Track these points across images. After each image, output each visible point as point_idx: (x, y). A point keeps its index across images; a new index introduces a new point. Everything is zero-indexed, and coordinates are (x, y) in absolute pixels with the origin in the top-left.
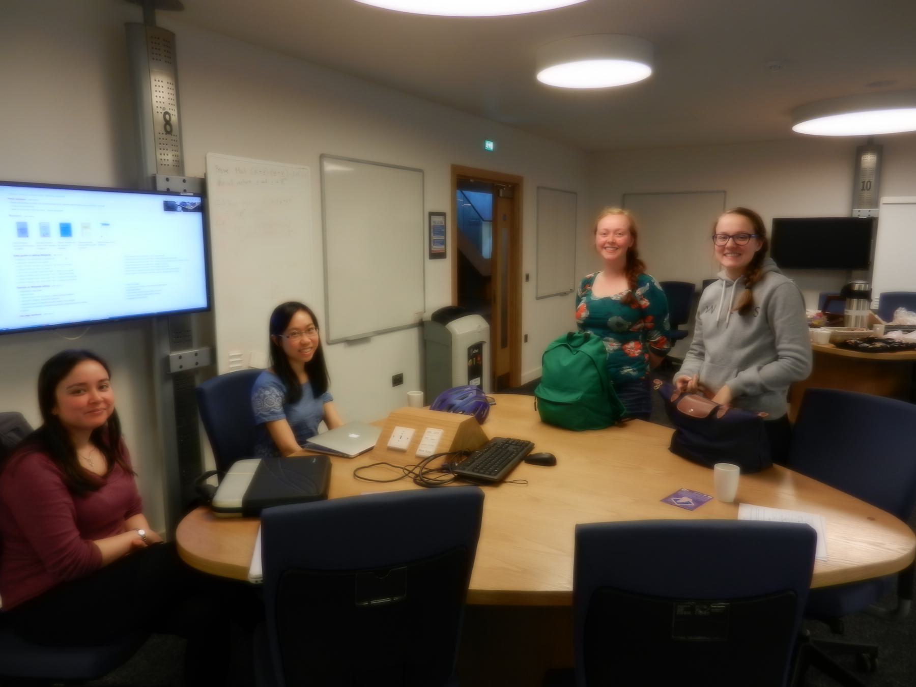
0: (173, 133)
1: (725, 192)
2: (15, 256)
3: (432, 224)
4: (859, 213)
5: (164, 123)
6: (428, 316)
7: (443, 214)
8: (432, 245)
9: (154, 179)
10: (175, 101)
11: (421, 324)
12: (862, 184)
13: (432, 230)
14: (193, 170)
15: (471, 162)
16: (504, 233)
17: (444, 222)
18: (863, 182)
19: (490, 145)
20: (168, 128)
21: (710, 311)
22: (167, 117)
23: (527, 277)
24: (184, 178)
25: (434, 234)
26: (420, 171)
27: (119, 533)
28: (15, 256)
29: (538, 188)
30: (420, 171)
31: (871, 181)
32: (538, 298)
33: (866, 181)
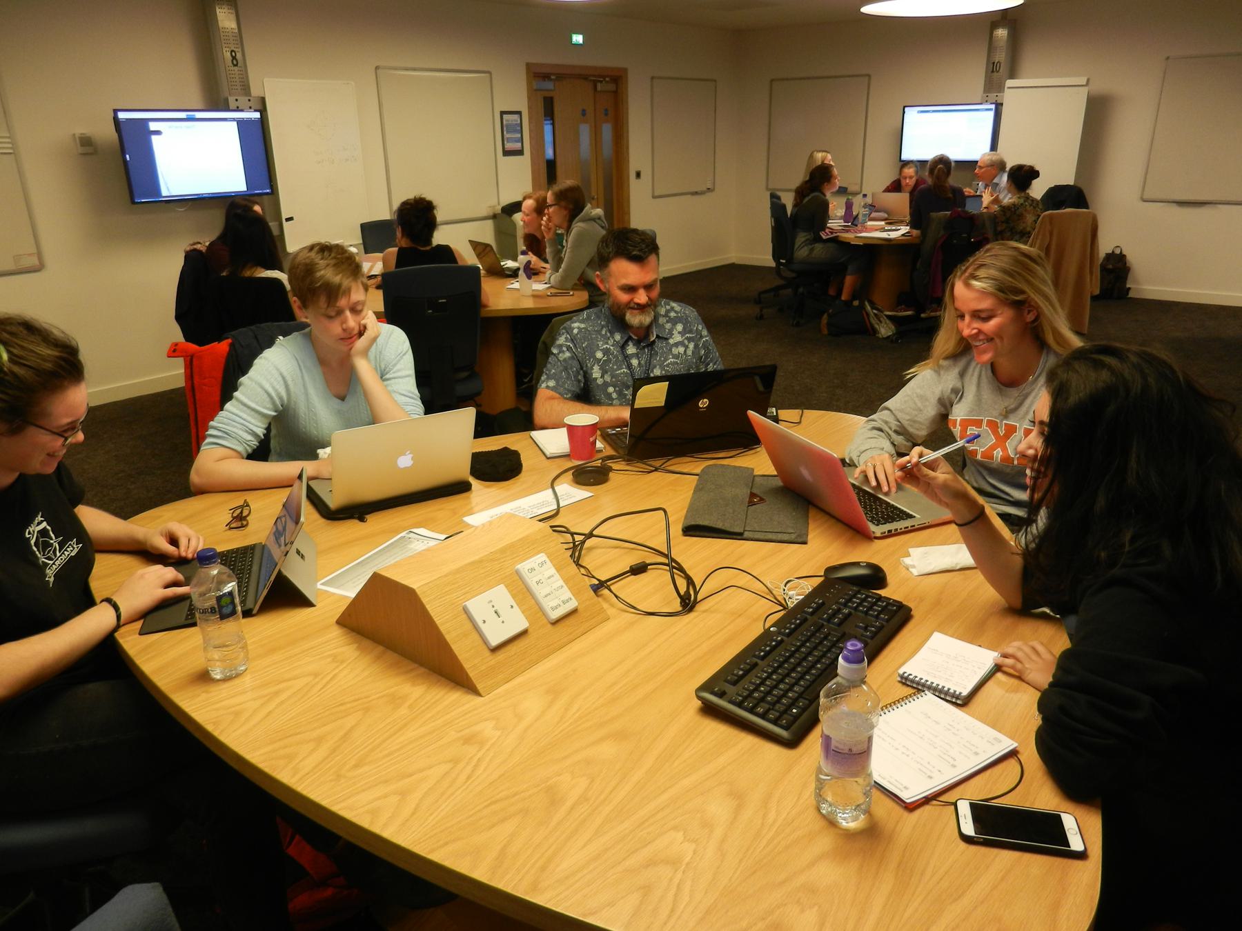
0: (239, 65)
1: (869, 76)
2: (303, 557)
3: (504, 122)
4: (997, 98)
5: (231, 58)
6: (498, 209)
7: (519, 113)
8: (505, 143)
9: (226, 100)
10: (238, 38)
11: (494, 217)
13: (505, 129)
14: (255, 92)
15: (549, 58)
16: (607, 130)
17: (519, 120)
18: (994, 63)
19: (578, 39)
20: (235, 62)
21: (77, 136)
22: (233, 54)
23: (638, 175)
24: (249, 98)
25: (507, 132)
26: (489, 72)
27: (342, 595)
28: (303, 557)
29: (653, 78)
30: (489, 72)
32: (654, 197)
33: (997, 61)
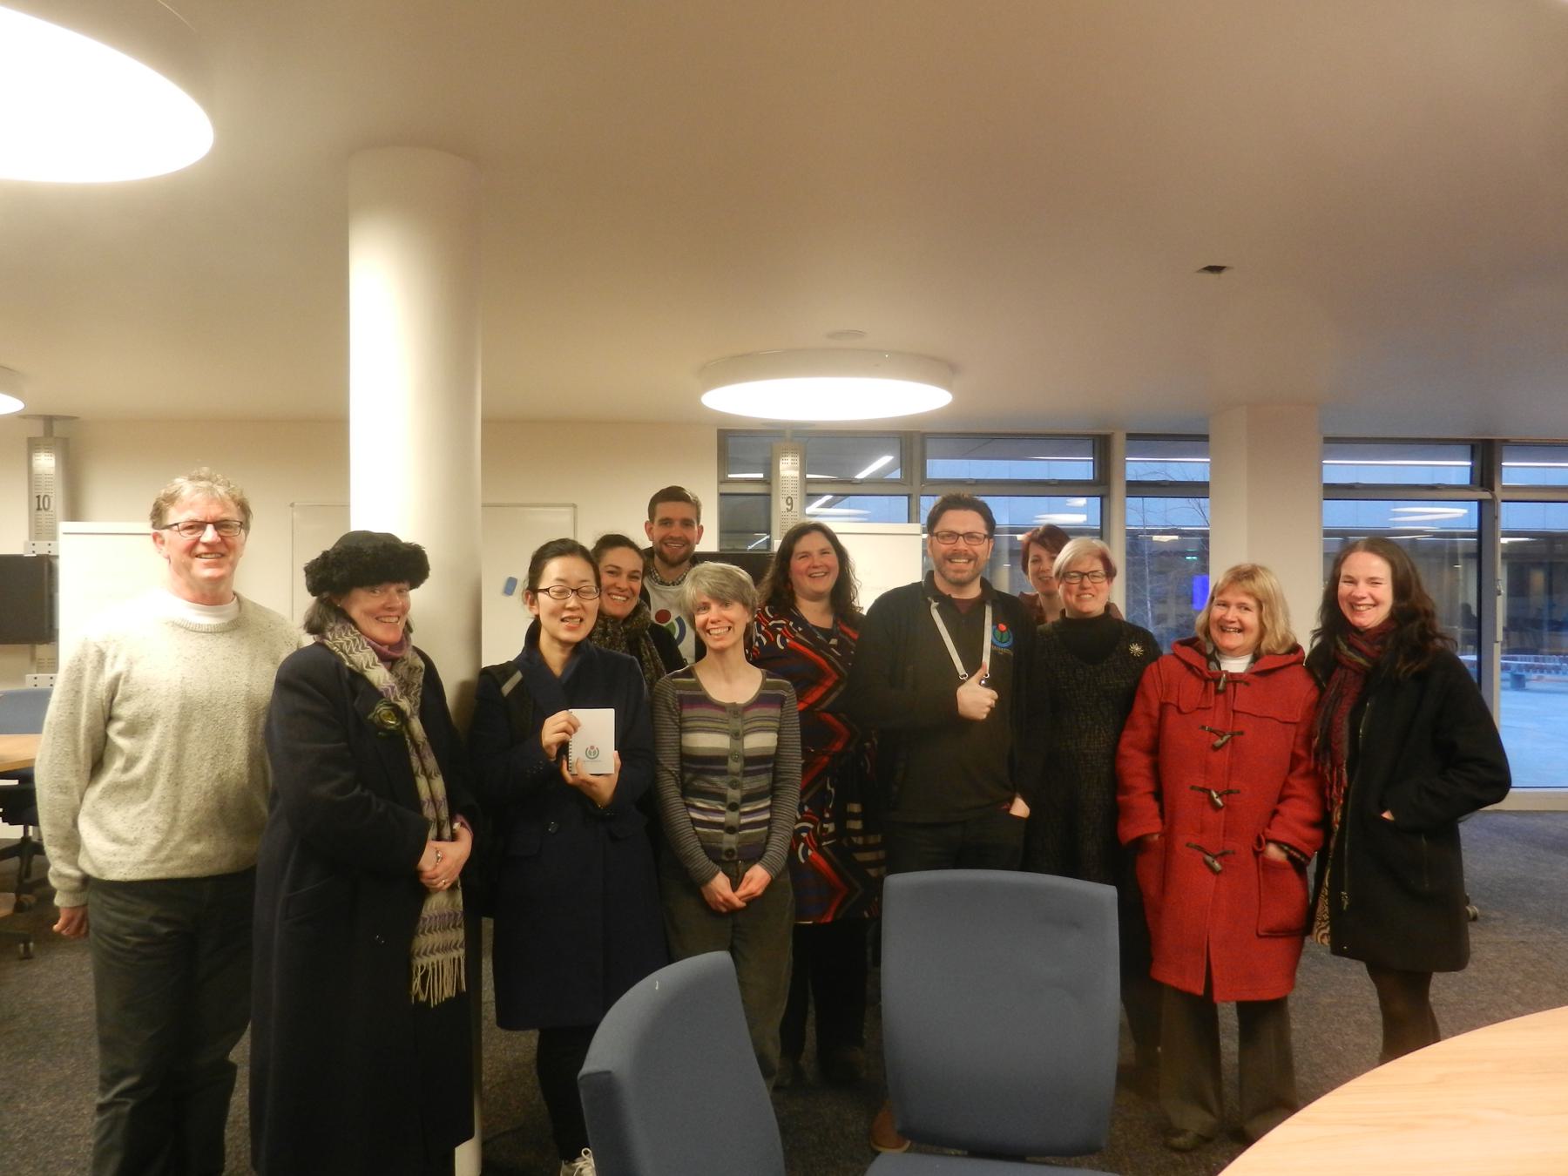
12: (37, 499)
18: (38, 497)
31: (50, 495)
33: (42, 495)
